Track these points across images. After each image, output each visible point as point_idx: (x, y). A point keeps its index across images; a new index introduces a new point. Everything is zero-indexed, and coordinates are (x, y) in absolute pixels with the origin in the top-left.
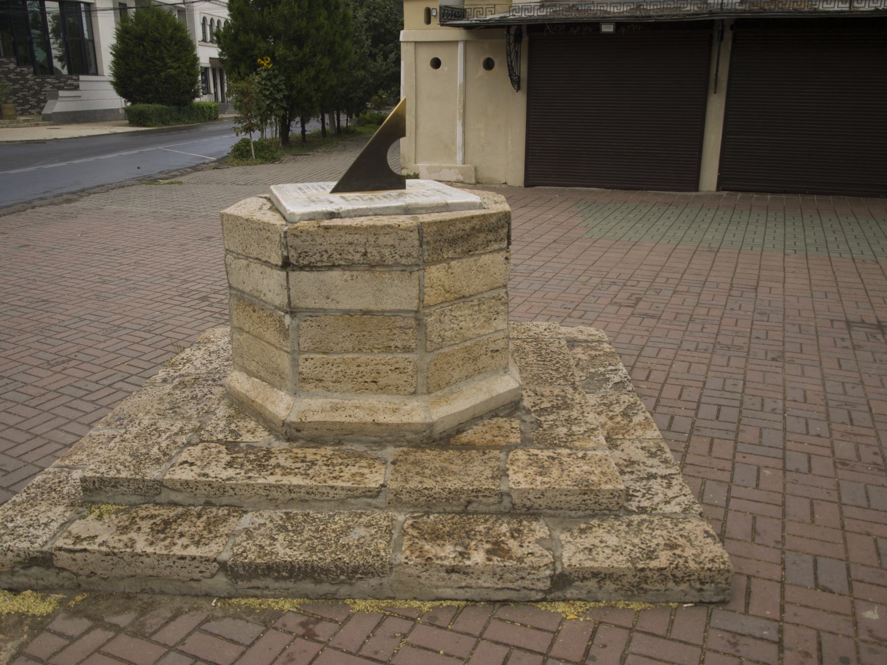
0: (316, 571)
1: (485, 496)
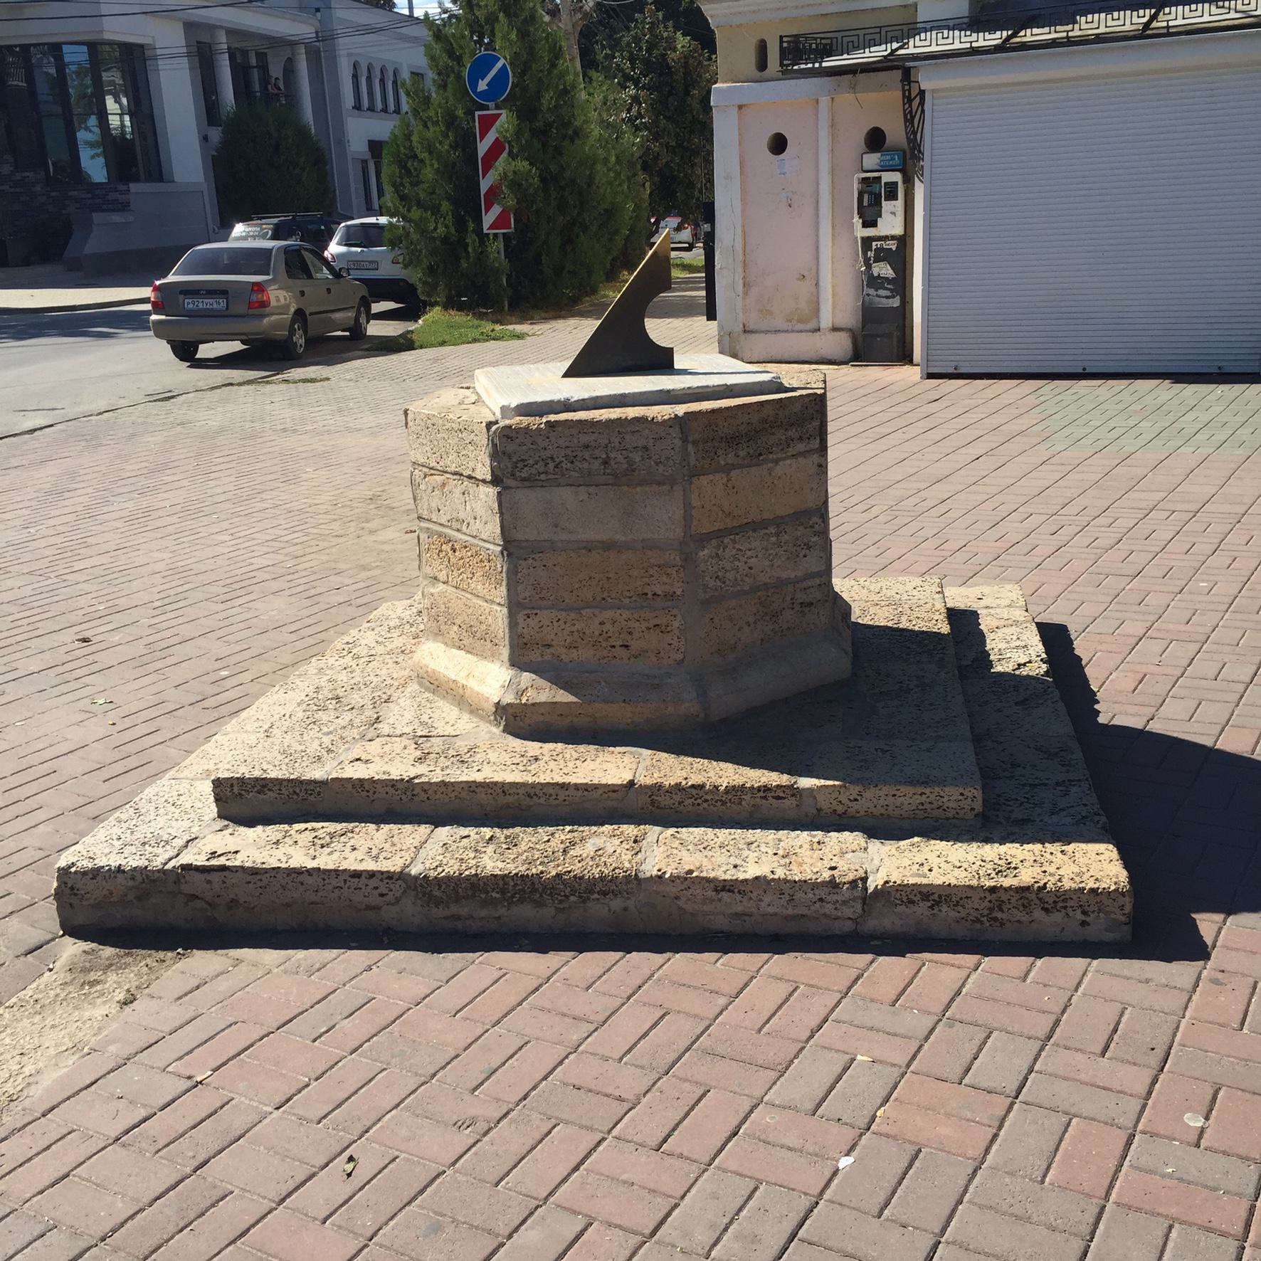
0: (537, 890)
1: (778, 798)
